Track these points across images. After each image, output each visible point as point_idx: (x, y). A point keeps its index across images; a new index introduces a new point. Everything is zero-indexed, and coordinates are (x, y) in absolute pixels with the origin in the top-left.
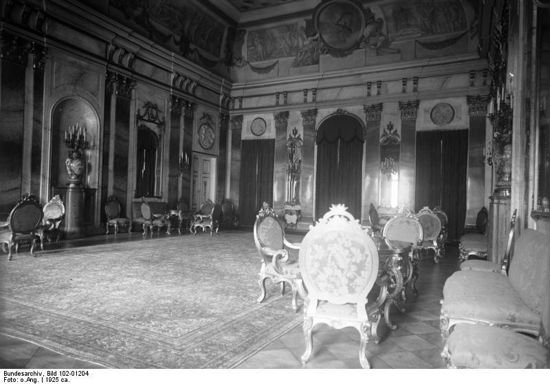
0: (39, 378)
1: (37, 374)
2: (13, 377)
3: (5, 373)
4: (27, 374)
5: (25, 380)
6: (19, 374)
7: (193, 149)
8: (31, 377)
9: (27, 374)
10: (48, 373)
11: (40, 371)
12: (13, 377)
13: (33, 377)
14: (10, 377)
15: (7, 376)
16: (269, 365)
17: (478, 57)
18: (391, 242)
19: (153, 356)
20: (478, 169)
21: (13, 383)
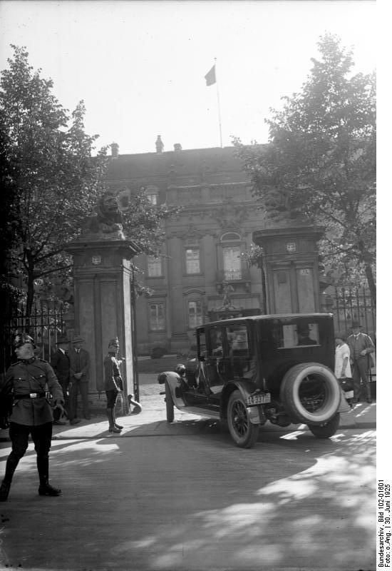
1: (382, 533)
2: (385, 557)
3: (381, 566)
4: (382, 543)
6: (381, 551)
7: (154, 150)
8: (385, 539)
9: (382, 543)
10: (381, 521)
12: (385, 557)
13: (385, 536)
14: (385, 561)
15: (384, 564)
16: (369, 316)
17: (184, 405)
18: (271, 137)
19: (343, 311)
20: (285, 327)
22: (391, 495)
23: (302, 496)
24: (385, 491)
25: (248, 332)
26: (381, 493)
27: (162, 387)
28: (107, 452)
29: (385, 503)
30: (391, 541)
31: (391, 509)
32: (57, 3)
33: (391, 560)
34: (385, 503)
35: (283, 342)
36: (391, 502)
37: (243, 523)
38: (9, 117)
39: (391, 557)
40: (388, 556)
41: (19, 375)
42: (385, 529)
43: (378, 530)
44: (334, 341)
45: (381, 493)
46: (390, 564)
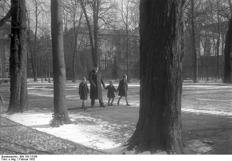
0: (16, 159)
1: (16, 157)
2: (6, 158)
3: (2, 156)
4: (11, 157)
5: (11, 159)
6: (8, 157)
8: (13, 158)
9: (11, 157)
10: (20, 156)
11: (17, 155)
12: (6, 158)
13: (14, 158)
14: (4, 158)
15: (3, 158)
21: (6, 160)
23: (59, 42)
24: (33, 158)
26: (33, 157)
28: (31, 113)
34: (27, 158)
37: (62, 71)
38: (196, 22)
41: (228, 28)
44: (140, 106)
45: (33, 157)
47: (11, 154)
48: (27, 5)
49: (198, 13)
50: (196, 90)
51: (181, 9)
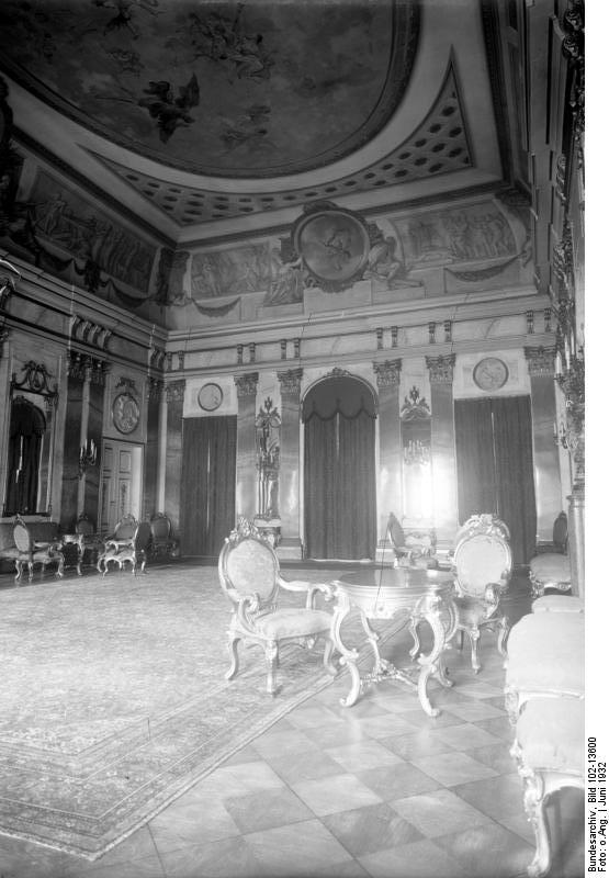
1: (594, 819)
2: (598, 857)
3: (592, 870)
4: (593, 835)
5: (602, 838)
6: (593, 847)
8: (598, 829)
9: (593, 835)
10: (592, 800)
11: (587, 815)
12: (598, 857)
13: (598, 825)
14: (598, 863)
22: (607, 779)
25: (375, 546)
27: (328, 703)
29: (598, 792)
30: (607, 832)
31: (607, 800)
32: (268, 847)
33: (607, 861)
34: (598, 792)
35: (398, 390)
36: (607, 790)
39: (607, 857)
40: (603, 855)
42: (598, 813)
43: (587, 792)
46: (607, 868)
47: (289, 299)
48: (178, 507)
49: (71, 807)
50: (334, 434)
51: (279, 537)
